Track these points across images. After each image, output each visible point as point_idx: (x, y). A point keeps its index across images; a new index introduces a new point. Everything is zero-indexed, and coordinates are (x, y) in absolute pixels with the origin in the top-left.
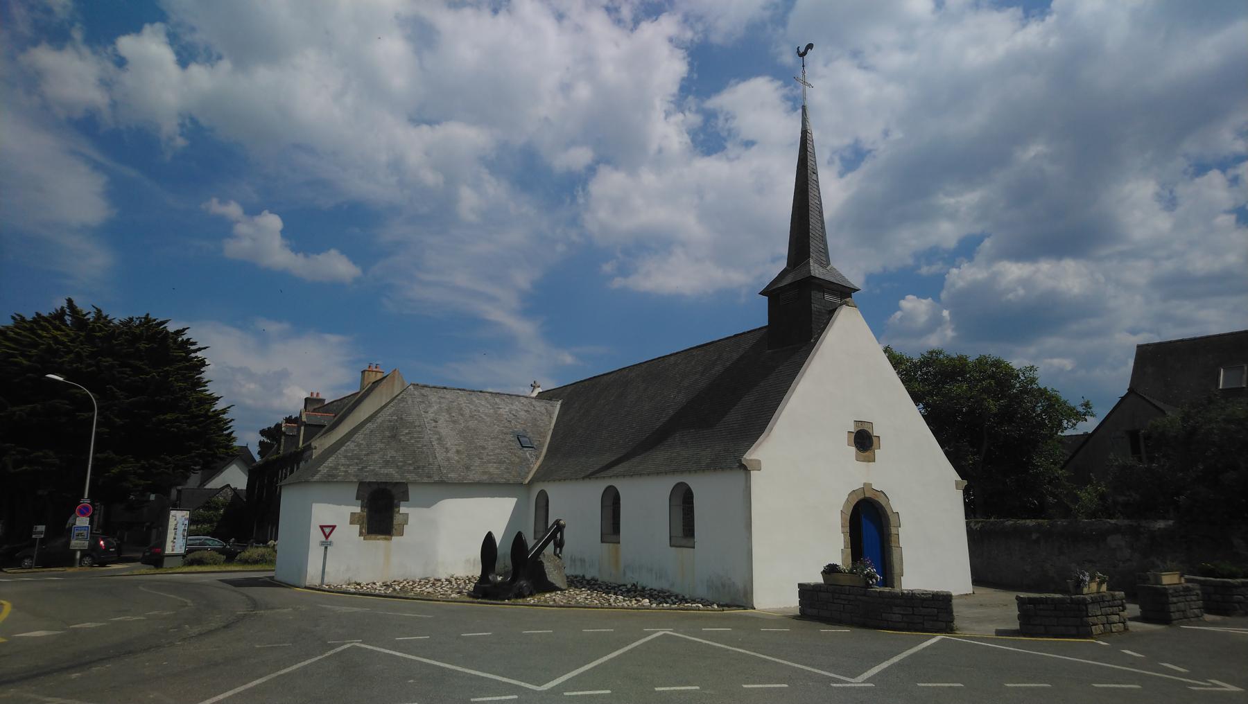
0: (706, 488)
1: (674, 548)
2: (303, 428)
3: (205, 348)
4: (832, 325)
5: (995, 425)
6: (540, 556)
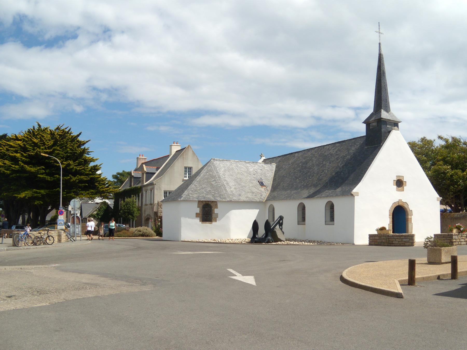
0: (339, 203)
1: (326, 225)
2: (145, 175)
3: (68, 127)
4: (389, 138)
5: (331, 194)
6: (275, 229)
